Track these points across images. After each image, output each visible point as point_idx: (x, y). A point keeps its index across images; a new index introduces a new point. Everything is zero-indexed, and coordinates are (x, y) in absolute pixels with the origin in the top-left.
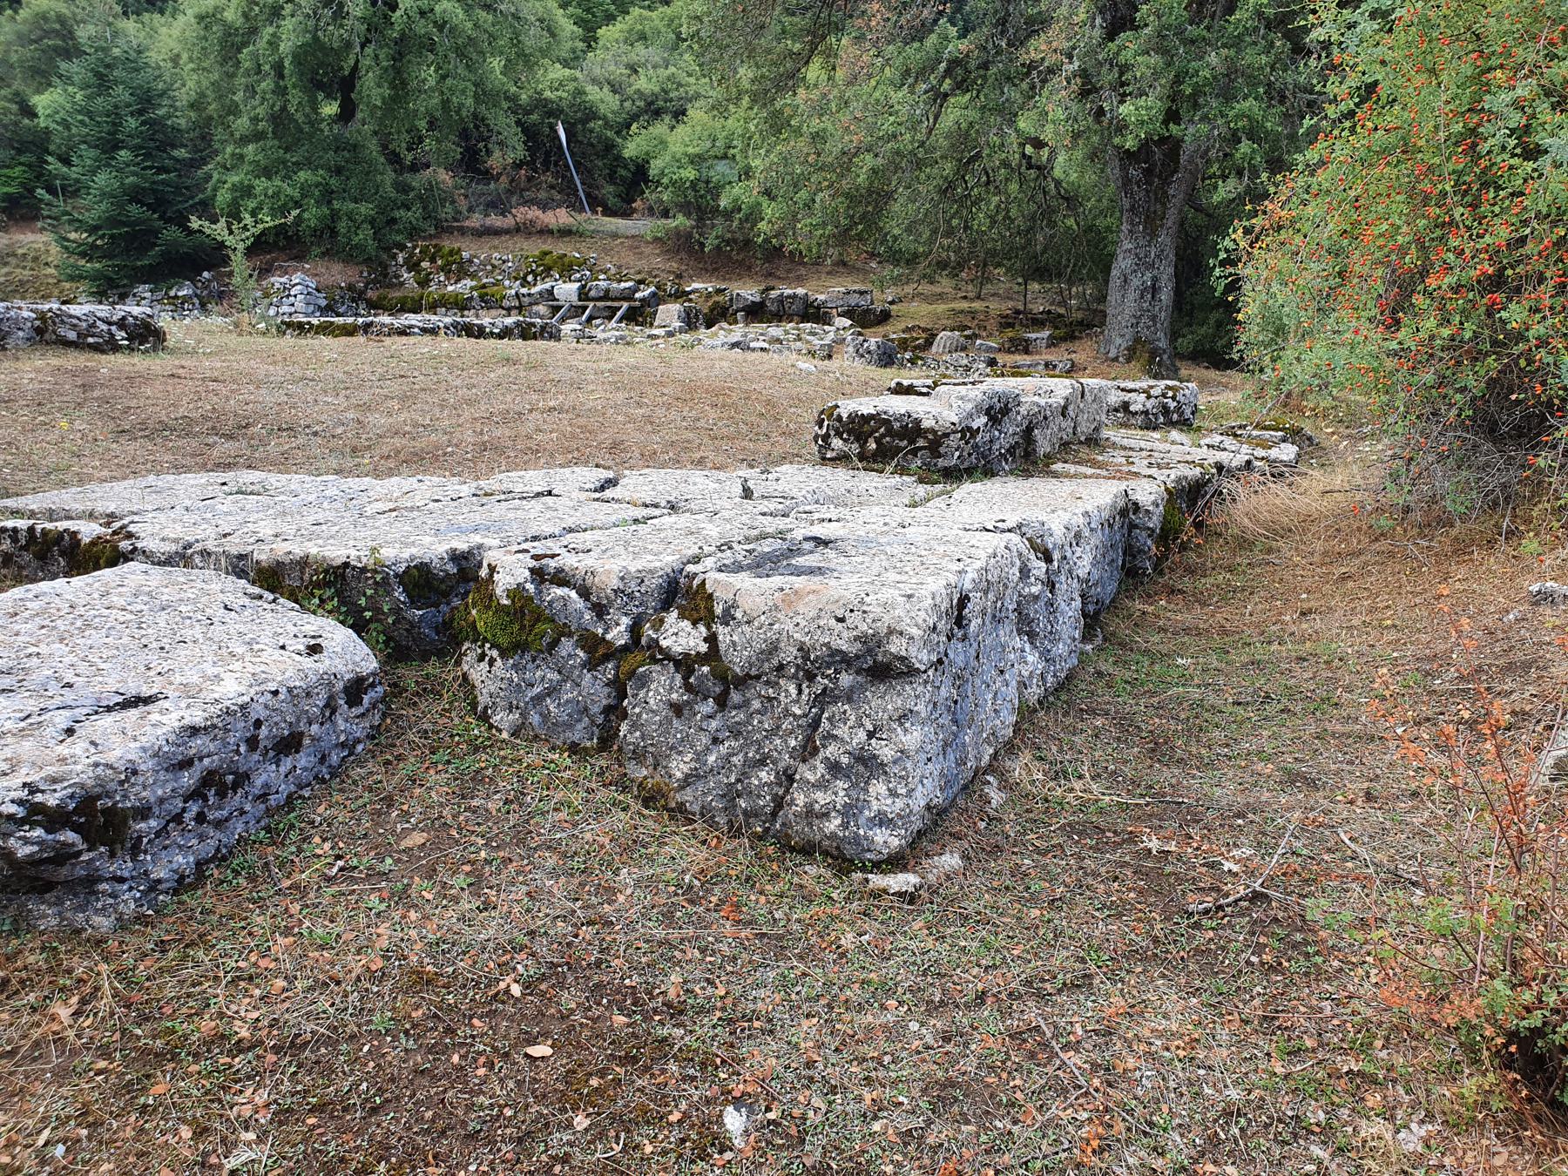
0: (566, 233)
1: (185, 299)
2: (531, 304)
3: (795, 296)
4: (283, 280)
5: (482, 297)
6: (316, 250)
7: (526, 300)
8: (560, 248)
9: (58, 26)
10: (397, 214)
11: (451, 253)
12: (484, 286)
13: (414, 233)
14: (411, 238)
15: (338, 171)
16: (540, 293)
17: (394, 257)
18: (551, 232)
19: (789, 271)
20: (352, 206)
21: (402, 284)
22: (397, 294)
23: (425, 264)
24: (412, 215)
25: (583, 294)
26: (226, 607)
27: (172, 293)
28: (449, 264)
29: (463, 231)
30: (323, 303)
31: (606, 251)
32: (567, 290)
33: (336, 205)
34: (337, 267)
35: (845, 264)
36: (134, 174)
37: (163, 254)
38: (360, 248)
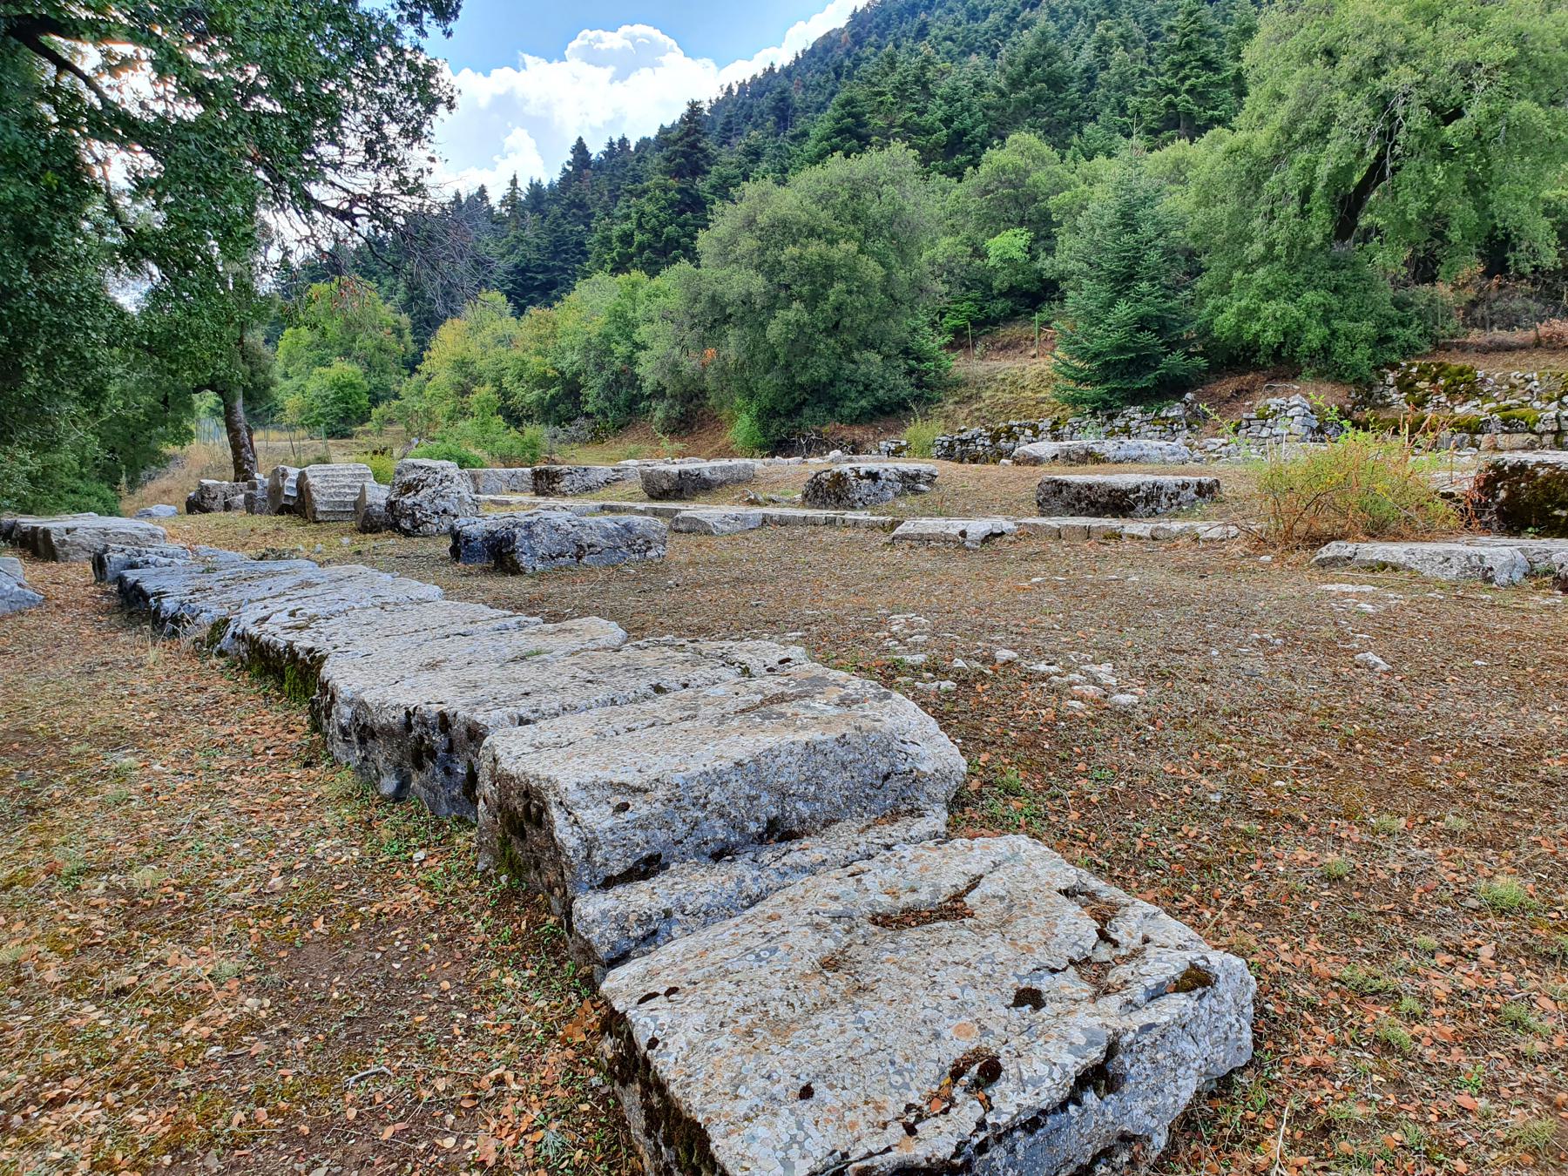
1: (1175, 420)
4: (1280, 401)
5: (1505, 421)
6: (1307, 371)
10: (1393, 332)
11: (1461, 372)
12: (1508, 408)
13: (1409, 350)
15: (1336, 290)
17: (1382, 377)
20: (1351, 325)
21: (1389, 405)
24: (1410, 334)
26: (788, 660)
29: (1463, 348)
30: (1316, 424)
33: (1336, 324)
38: (1354, 368)
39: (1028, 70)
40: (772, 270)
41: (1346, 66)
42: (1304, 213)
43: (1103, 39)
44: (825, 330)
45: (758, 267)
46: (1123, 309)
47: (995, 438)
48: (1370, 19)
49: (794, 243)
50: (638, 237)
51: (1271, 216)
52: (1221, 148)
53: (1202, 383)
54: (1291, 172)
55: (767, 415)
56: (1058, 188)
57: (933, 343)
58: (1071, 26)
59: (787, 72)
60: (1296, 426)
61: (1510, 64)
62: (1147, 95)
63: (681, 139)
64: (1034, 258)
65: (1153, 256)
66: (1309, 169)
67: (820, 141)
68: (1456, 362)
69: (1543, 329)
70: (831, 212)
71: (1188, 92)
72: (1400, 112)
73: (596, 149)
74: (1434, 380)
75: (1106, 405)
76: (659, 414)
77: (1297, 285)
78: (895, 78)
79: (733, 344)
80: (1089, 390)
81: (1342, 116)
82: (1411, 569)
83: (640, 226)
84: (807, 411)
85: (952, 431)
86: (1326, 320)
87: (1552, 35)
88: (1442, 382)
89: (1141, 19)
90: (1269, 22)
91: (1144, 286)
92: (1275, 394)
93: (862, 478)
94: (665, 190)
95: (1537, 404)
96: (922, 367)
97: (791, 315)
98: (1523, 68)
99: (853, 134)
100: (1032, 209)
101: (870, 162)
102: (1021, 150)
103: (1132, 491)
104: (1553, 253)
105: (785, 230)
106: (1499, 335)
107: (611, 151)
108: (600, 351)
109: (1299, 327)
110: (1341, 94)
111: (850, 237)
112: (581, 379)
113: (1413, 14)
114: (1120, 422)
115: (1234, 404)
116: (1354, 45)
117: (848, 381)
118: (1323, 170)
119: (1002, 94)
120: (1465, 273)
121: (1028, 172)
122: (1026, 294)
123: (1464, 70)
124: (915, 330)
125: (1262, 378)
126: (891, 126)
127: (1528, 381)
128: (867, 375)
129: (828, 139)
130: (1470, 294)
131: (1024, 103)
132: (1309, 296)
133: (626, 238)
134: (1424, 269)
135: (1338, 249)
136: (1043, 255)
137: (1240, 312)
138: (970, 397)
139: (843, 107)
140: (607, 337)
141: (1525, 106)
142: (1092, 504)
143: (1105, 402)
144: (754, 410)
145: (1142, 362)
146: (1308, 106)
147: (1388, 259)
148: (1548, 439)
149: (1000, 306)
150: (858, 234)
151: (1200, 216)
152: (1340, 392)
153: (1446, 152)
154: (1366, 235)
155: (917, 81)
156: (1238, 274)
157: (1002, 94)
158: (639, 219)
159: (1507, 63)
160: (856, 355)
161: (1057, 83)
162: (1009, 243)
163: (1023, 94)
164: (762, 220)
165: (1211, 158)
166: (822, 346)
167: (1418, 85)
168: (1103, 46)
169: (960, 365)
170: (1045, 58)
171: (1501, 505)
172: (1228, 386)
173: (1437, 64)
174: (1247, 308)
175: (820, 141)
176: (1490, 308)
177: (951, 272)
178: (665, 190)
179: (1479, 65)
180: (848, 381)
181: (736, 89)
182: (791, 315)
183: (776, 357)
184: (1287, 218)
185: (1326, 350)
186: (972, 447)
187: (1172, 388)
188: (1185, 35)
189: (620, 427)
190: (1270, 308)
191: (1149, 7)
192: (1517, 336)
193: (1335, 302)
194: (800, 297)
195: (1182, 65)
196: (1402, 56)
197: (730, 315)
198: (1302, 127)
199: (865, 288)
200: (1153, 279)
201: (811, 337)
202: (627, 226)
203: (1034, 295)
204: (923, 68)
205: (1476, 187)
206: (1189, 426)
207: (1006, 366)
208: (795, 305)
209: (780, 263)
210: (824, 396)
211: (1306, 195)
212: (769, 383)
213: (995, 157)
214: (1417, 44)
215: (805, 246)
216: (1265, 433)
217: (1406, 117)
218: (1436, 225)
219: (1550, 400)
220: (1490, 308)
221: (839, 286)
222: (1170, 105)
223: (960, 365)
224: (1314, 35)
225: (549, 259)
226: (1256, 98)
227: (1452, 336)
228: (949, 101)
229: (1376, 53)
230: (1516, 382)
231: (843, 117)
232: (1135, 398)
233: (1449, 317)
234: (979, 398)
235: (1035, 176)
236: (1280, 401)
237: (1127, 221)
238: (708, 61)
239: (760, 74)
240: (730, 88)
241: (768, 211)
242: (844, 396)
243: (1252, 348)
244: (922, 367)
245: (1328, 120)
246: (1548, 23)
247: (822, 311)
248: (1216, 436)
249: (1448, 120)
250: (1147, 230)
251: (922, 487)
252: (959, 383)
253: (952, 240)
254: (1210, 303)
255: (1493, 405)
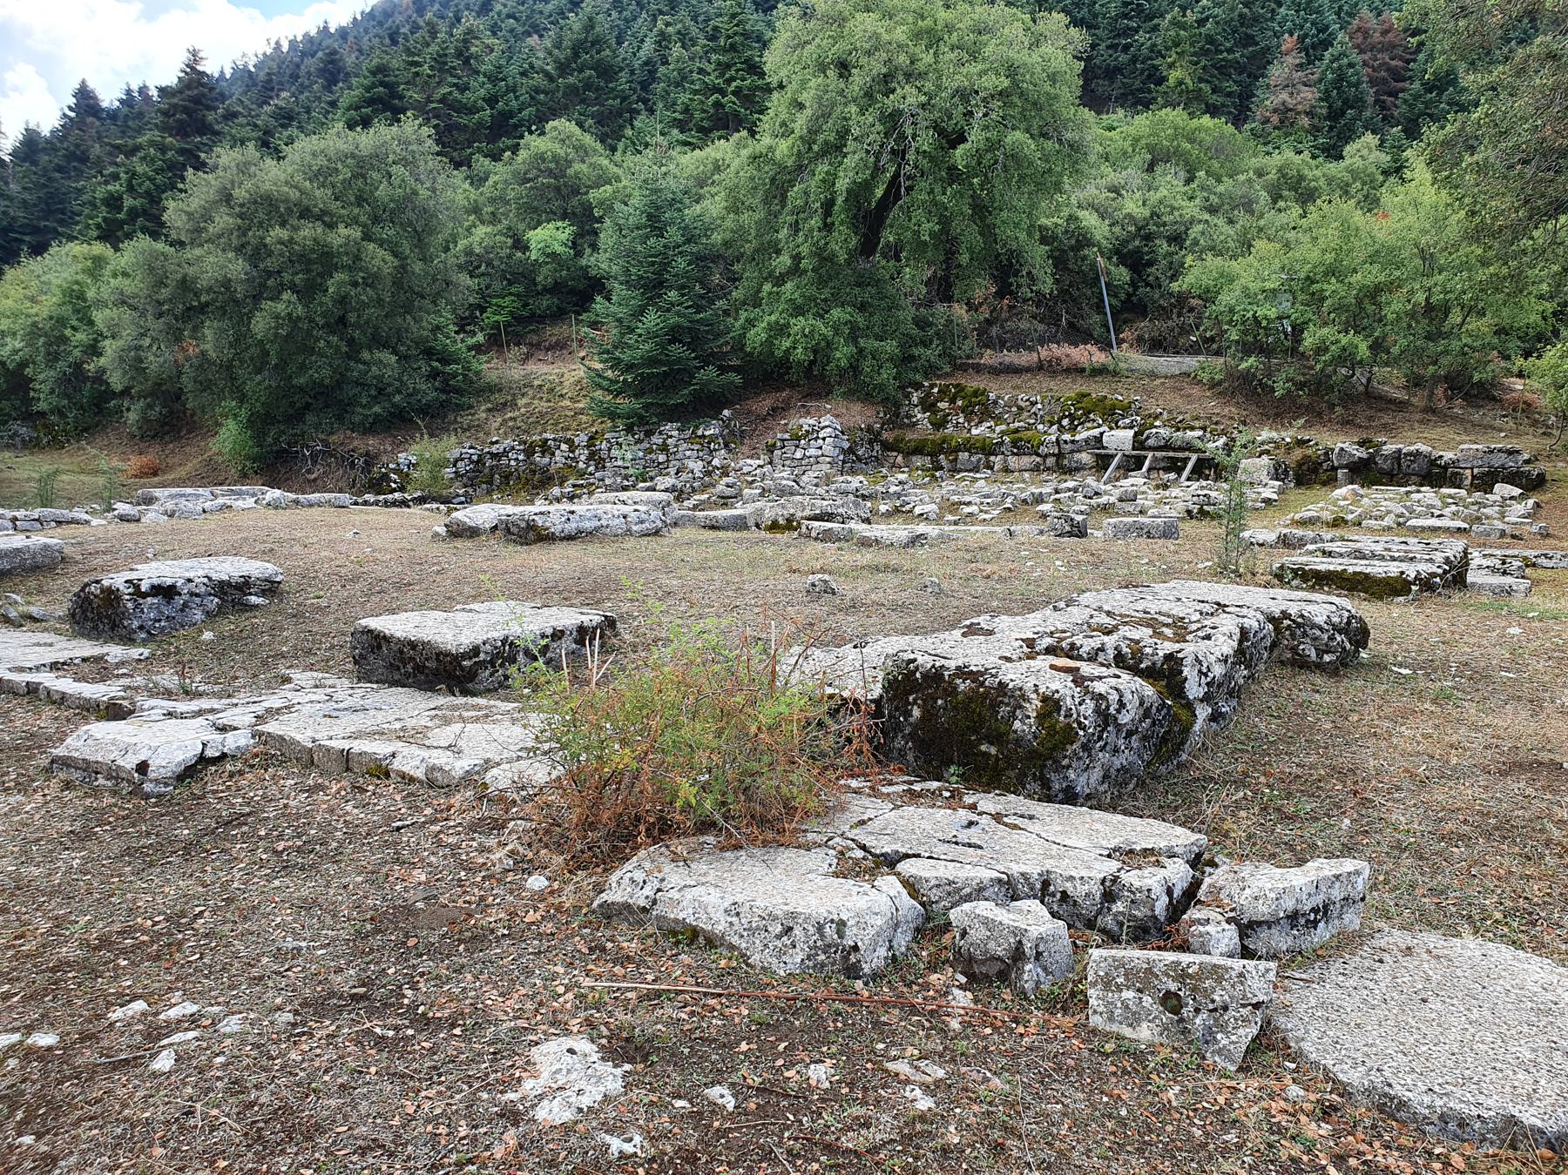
0: (1100, 372)
1: (712, 439)
2: (1072, 451)
3: (1418, 453)
5: (1014, 443)
7: (1068, 447)
8: (1098, 389)
9: (552, 166)
11: (976, 393)
12: (1017, 431)
13: (931, 370)
14: (926, 376)
15: (862, 307)
16: (1087, 441)
17: (908, 396)
18: (1083, 370)
19: (1371, 419)
21: (915, 424)
22: (910, 436)
23: (942, 405)
24: (930, 353)
25: (1139, 443)
27: (700, 433)
28: (971, 404)
29: (978, 369)
30: (846, 445)
31: (1149, 393)
32: (1119, 439)
34: (857, 407)
35: (1434, 411)
36: (678, 314)
37: (694, 394)
38: (881, 387)
39: (576, 55)
40: (257, 254)
41: (858, 80)
42: (827, 227)
43: (662, 33)
44: (327, 324)
45: (239, 250)
46: (651, 319)
47: (529, 452)
48: (877, 36)
49: (283, 224)
50: (128, 202)
51: (795, 228)
52: (745, 153)
53: (741, 399)
54: (813, 184)
55: (259, 424)
56: (603, 180)
57: (459, 344)
58: (635, 18)
59: (343, 33)
60: (828, 448)
61: (1002, 94)
62: (696, 92)
63: (181, 92)
64: (579, 254)
65: (681, 263)
66: (829, 182)
67: (348, 109)
68: (973, 383)
69: (1044, 353)
70: (329, 192)
71: (733, 93)
72: (909, 132)
73: (109, 97)
74: (953, 401)
75: (642, 421)
76: (132, 417)
77: (825, 300)
78: (434, 48)
79: (210, 339)
80: (625, 403)
81: (856, 131)
82: (732, 947)
83: (131, 189)
84: (310, 418)
85: (483, 443)
86: (853, 338)
87: (1039, 69)
88: (960, 403)
89: (701, 19)
90: (787, 23)
91: (673, 295)
92: (808, 413)
93: (145, 595)
94: (163, 149)
95: (1040, 427)
96: (447, 369)
97: (280, 307)
98: (1015, 99)
99: (383, 102)
100: (575, 201)
101: (379, 136)
102: (558, 138)
103: (464, 656)
104: (1050, 281)
105: (269, 208)
106: (1010, 357)
107: (128, 101)
108: (51, 337)
109: (828, 344)
110: (854, 109)
111: (353, 221)
112: (28, 371)
113: (917, 35)
114: (657, 440)
115: (770, 422)
116: (863, 60)
117: (358, 384)
118: (842, 184)
119: (551, 79)
120: (978, 294)
121: (569, 163)
122: (572, 291)
123: (964, 95)
124: (438, 328)
125: (797, 396)
126: (428, 100)
127: (1034, 404)
128: (380, 378)
129: (357, 108)
130: (985, 313)
131: (572, 91)
132: (836, 313)
133: (113, 202)
134: (943, 289)
135: (862, 265)
136: (588, 251)
137: (770, 327)
138: (504, 405)
139: (374, 73)
140: (61, 321)
141: (1016, 137)
142: (420, 668)
143: (641, 417)
144: (244, 413)
145: (675, 376)
146: (826, 116)
147: (913, 277)
148: (1051, 461)
149: (545, 302)
150: (363, 219)
151: (729, 223)
152: (870, 412)
153: (953, 175)
154: (894, 252)
155: (459, 54)
156: (767, 287)
157: (551, 79)
158: (129, 181)
159: (1001, 93)
160: (366, 355)
161: (607, 72)
162: (550, 236)
163: (571, 80)
164: (240, 194)
165: (736, 164)
166: (322, 344)
167: (923, 106)
168: (663, 40)
169: (492, 368)
170: (593, 44)
171: (915, 726)
172: (764, 404)
173: (939, 87)
174: (777, 323)
175: (348, 109)
176: (1002, 327)
177: (489, 264)
178: (163, 149)
179: (977, 92)
180: (358, 384)
181: (285, 48)
182: (280, 307)
183: (268, 354)
184: (811, 230)
185: (854, 368)
186: (504, 461)
187: (705, 405)
188: (729, 37)
189: (85, 430)
190: (799, 324)
191: (705, 7)
192: (1024, 358)
193: (860, 319)
194: (293, 288)
195: (728, 66)
196: (908, 76)
197: (207, 304)
198: (821, 138)
199: (372, 280)
200: (683, 287)
201: (309, 333)
202: (114, 187)
203: (578, 292)
204: (465, 41)
205: (981, 211)
206: (726, 445)
207: (543, 370)
208: (285, 296)
209: (265, 246)
210: (332, 400)
211: (828, 206)
212: (258, 384)
213: (534, 144)
214: (921, 66)
215: (296, 229)
216: (798, 455)
217: (914, 136)
218: (947, 243)
219: (1052, 424)
220: (1002, 327)
221: (339, 276)
222: (717, 104)
223: (492, 368)
224: (823, 45)
225: (39, 219)
226: (777, 104)
227: (968, 357)
228: (493, 78)
229: (884, 70)
230: (1023, 404)
231: (374, 86)
232: (672, 414)
233: (966, 338)
234: (514, 406)
235: (577, 166)
236: (812, 422)
237: (654, 222)
238: (255, 13)
239: (313, 32)
240: (277, 43)
241: (248, 185)
242: (353, 402)
243: (785, 363)
244: (447, 369)
245: (843, 134)
246: (1035, 58)
247: (321, 304)
248: (752, 457)
249: (953, 145)
250: (674, 234)
251: (254, 599)
252: (493, 389)
253: (489, 230)
254: (743, 315)
255: (1004, 427)
